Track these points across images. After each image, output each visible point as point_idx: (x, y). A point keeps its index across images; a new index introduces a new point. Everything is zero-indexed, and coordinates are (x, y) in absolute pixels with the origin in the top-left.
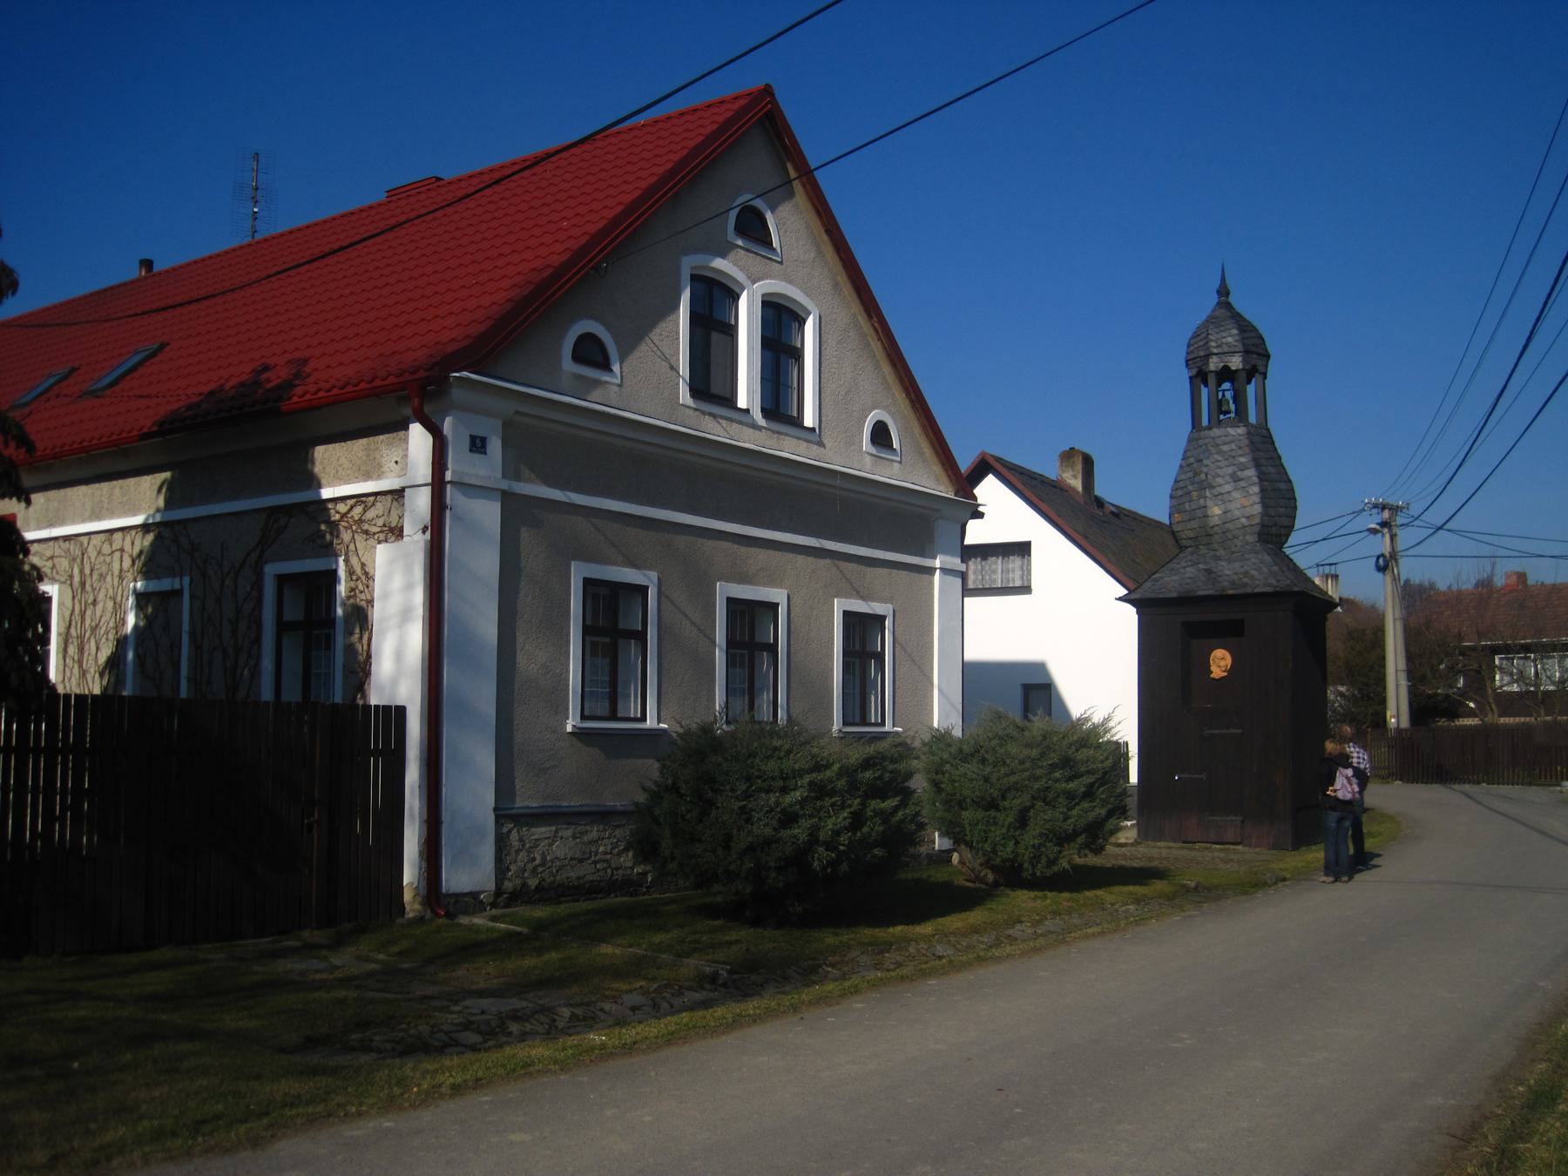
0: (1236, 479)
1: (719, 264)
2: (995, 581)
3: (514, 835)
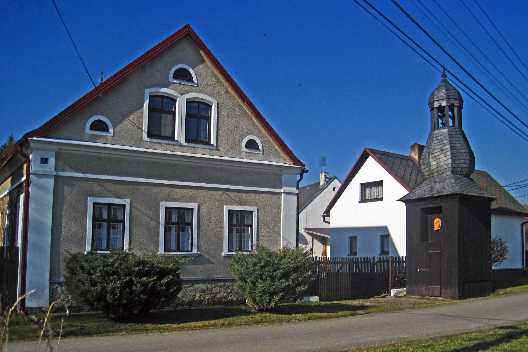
0: (442, 150)
1: (164, 90)
2: (374, 196)
3: (59, 289)
